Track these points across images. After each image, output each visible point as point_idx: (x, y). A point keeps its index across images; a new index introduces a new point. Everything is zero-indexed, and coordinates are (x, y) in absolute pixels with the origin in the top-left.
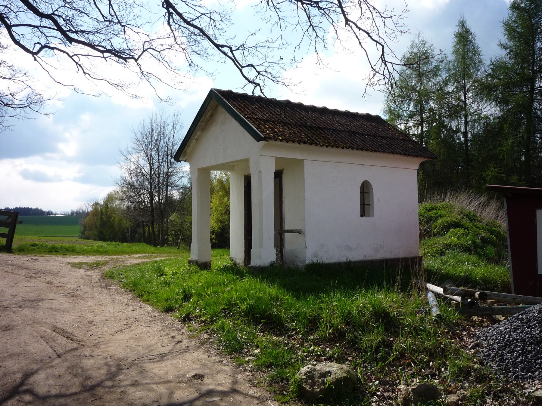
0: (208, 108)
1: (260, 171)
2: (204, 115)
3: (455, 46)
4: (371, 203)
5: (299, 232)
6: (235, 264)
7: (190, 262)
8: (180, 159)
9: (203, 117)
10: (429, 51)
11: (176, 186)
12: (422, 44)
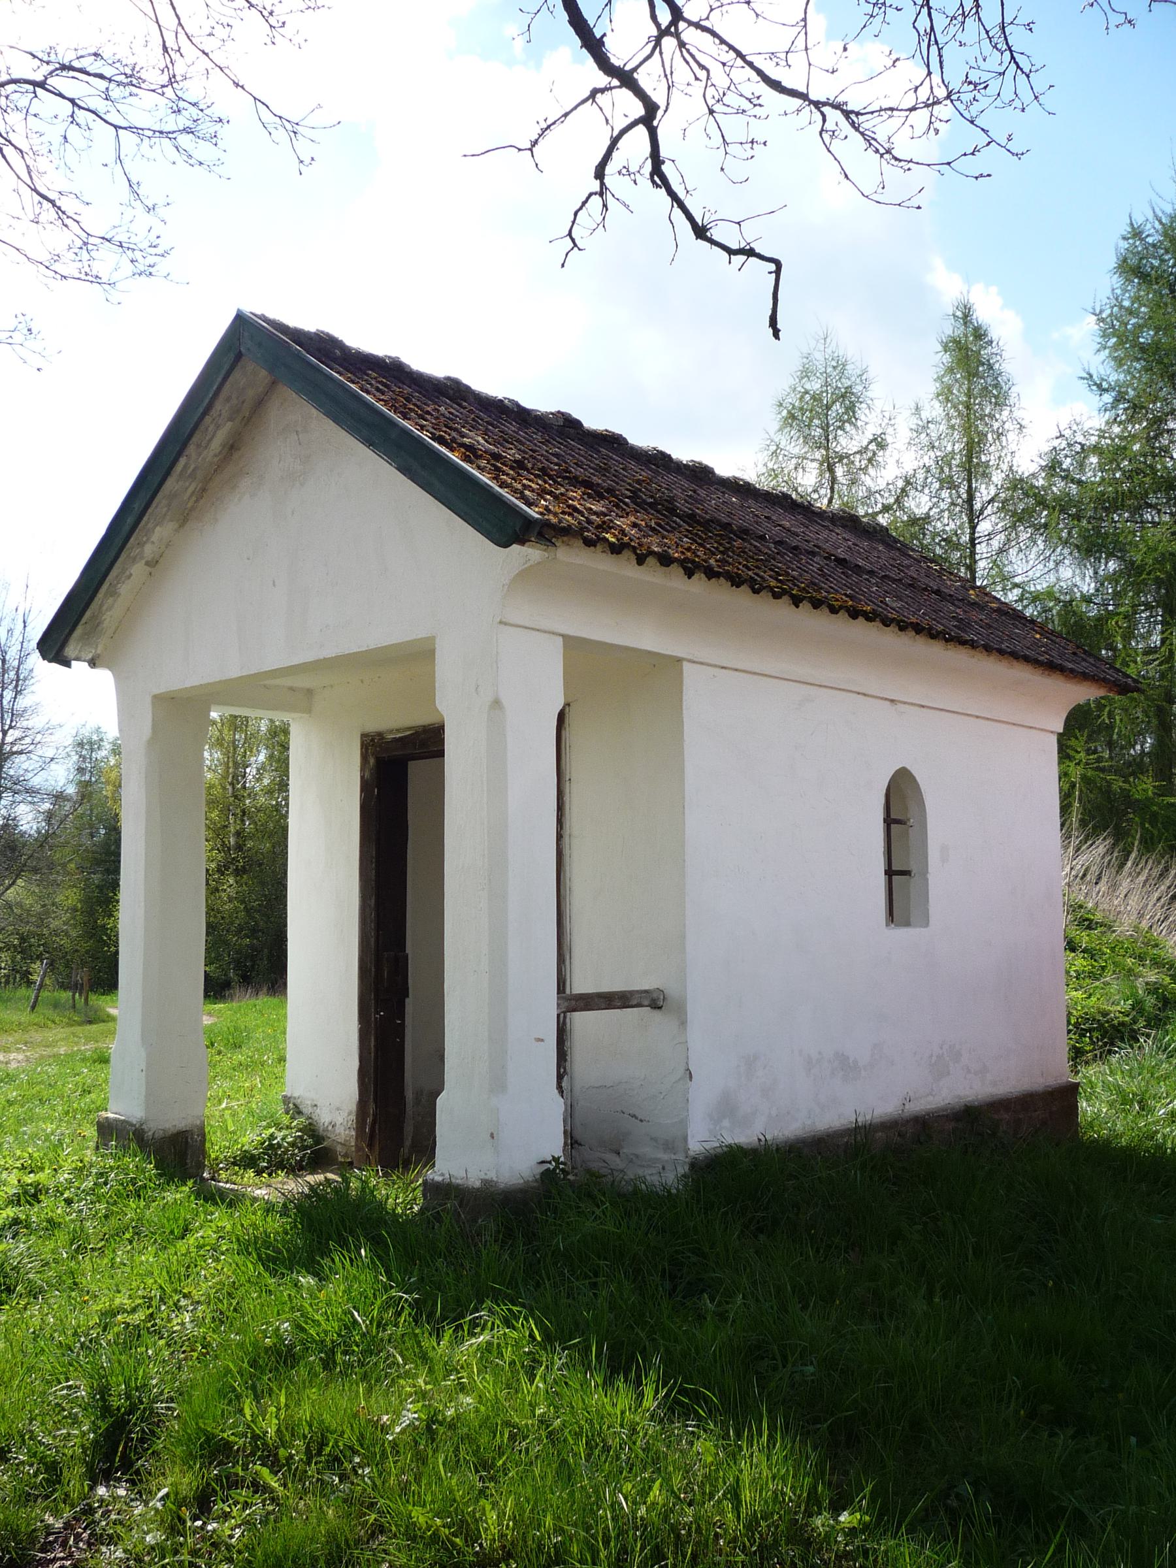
0: (218, 406)
1: (497, 704)
2: (194, 439)
3: (939, 379)
4: (913, 867)
5: (654, 1001)
6: (311, 1131)
7: (106, 1130)
8: (70, 651)
9: (191, 449)
10: (857, 389)
11: (31, 791)
12: (834, 368)
